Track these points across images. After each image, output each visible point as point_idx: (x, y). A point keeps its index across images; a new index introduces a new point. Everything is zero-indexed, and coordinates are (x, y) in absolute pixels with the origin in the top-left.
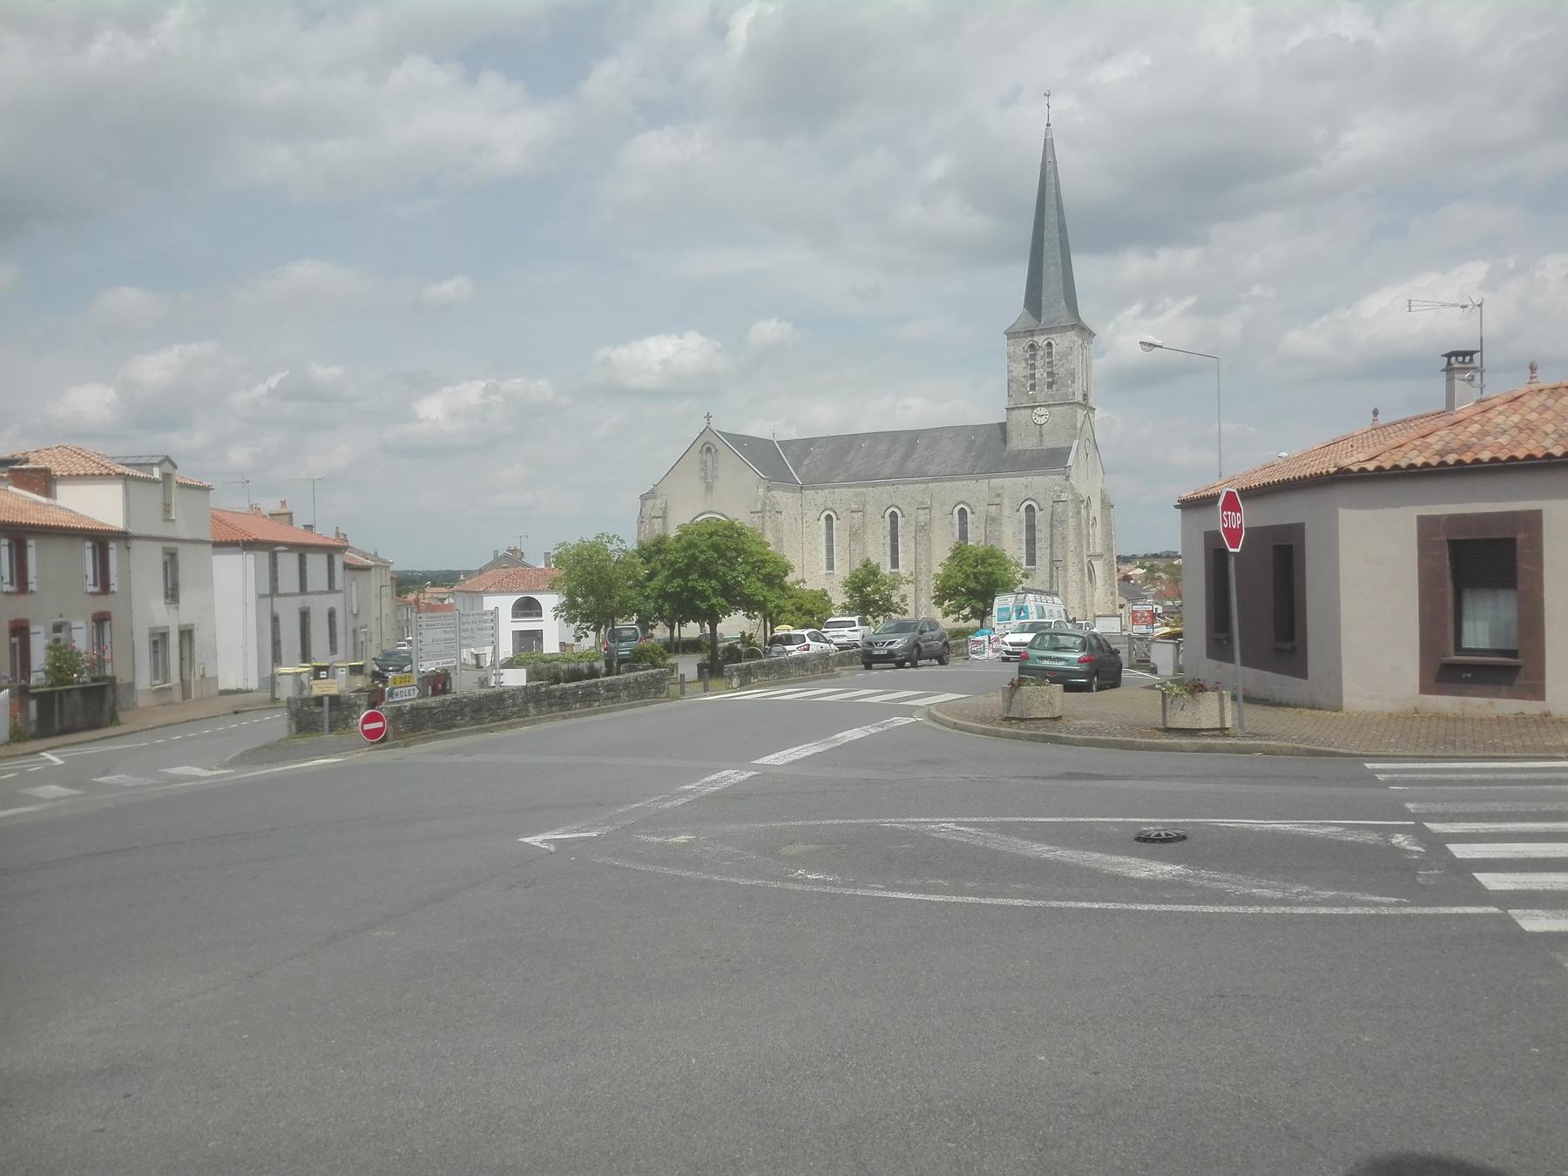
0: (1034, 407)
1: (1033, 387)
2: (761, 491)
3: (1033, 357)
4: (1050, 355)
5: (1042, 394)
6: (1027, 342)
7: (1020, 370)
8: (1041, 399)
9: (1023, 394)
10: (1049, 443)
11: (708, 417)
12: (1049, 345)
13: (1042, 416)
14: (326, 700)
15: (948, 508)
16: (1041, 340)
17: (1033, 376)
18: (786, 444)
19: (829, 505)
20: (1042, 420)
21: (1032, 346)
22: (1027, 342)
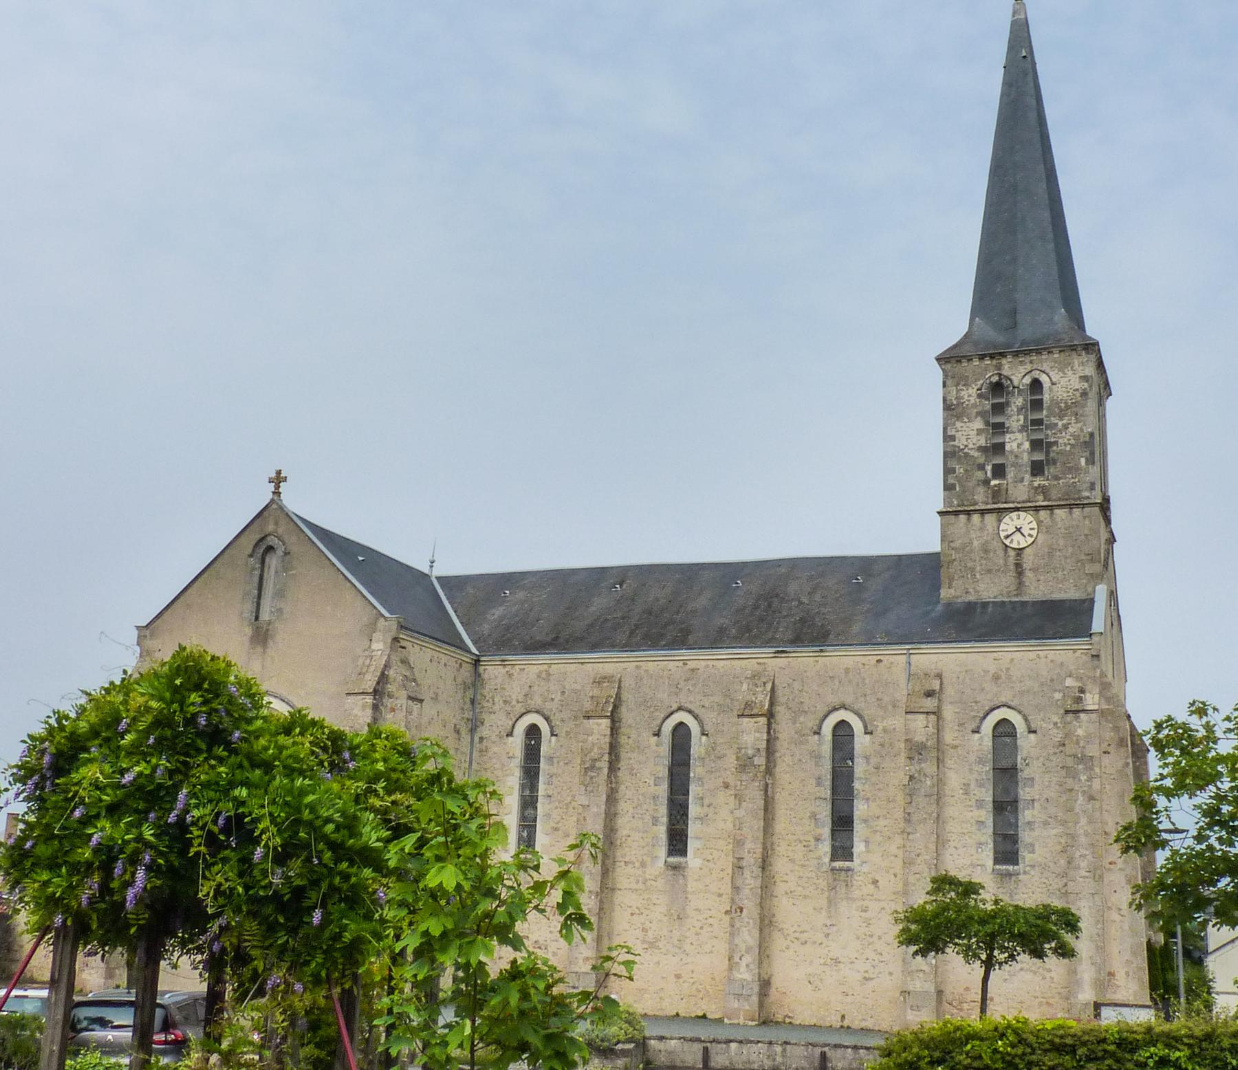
0: (1001, 512)
1: (999, 471)
2: (379, 645)
3: (999, 409)
4: (1037, 405)
5: (1020, 486)
6: (987, 372)
7: (971, 434)
8: (1020, 492)
9: (974, 485)
10: (1038, 589)
11: (278, 479)
12: (1036, 385)
13: (1020, 529)
14: (671, 860)
15: (811, 723)
16: (1018, 373)
17: (999, 448)
18: (453, 584)
19: (537, 701)
20: (1018, 541)
21: (998, 388)
22: (987, 372)
